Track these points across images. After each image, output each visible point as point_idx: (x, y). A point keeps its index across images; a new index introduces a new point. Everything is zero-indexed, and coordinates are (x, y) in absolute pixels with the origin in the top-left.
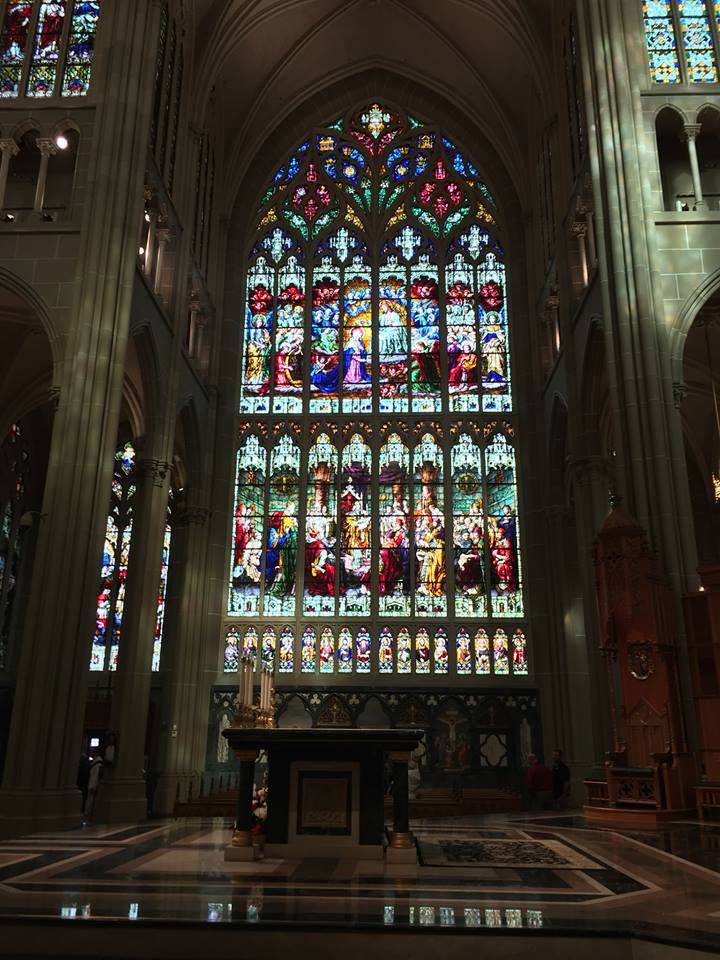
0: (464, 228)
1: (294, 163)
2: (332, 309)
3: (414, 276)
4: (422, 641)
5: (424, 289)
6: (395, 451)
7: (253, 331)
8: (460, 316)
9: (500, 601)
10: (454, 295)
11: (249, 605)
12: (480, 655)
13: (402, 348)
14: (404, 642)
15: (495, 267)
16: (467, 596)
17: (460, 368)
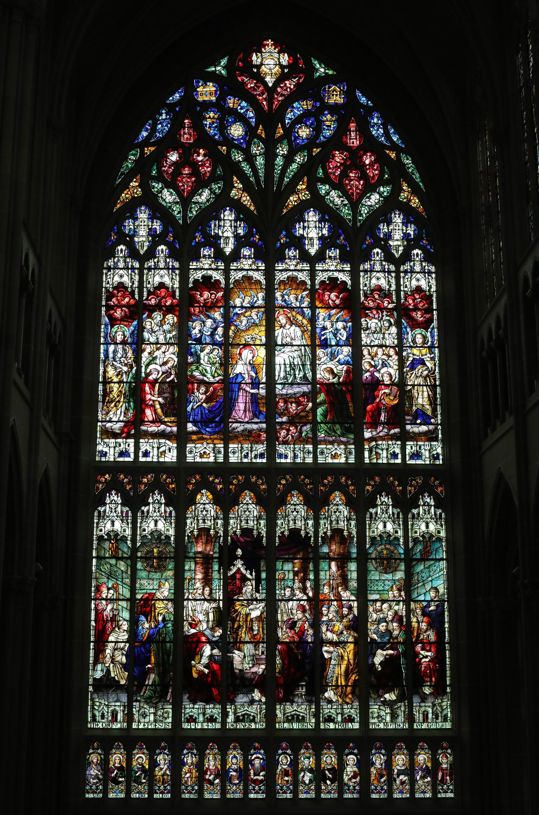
0: (382, 214)
1: (164, 116)
2: (214, 320)
3: (321, 277)
4: (329, 759)
5: (333, 295)
6: (295, 515)
7: (112, 348)
8: (379, 332)
9: (423, 709)
10: (371, 304)
11: (114, 714)
12: (398, 776)
13: (305, 376)
14: (307, 761)
15: (423, 268)
16: (385, 703)
17: (378, 404)
